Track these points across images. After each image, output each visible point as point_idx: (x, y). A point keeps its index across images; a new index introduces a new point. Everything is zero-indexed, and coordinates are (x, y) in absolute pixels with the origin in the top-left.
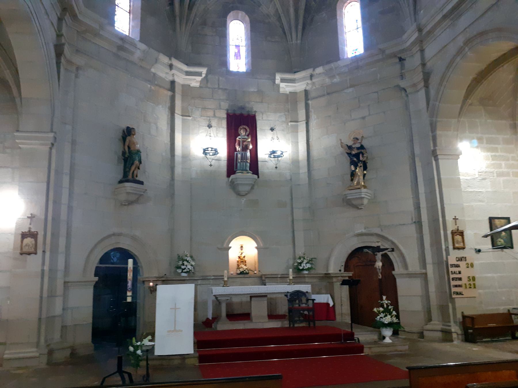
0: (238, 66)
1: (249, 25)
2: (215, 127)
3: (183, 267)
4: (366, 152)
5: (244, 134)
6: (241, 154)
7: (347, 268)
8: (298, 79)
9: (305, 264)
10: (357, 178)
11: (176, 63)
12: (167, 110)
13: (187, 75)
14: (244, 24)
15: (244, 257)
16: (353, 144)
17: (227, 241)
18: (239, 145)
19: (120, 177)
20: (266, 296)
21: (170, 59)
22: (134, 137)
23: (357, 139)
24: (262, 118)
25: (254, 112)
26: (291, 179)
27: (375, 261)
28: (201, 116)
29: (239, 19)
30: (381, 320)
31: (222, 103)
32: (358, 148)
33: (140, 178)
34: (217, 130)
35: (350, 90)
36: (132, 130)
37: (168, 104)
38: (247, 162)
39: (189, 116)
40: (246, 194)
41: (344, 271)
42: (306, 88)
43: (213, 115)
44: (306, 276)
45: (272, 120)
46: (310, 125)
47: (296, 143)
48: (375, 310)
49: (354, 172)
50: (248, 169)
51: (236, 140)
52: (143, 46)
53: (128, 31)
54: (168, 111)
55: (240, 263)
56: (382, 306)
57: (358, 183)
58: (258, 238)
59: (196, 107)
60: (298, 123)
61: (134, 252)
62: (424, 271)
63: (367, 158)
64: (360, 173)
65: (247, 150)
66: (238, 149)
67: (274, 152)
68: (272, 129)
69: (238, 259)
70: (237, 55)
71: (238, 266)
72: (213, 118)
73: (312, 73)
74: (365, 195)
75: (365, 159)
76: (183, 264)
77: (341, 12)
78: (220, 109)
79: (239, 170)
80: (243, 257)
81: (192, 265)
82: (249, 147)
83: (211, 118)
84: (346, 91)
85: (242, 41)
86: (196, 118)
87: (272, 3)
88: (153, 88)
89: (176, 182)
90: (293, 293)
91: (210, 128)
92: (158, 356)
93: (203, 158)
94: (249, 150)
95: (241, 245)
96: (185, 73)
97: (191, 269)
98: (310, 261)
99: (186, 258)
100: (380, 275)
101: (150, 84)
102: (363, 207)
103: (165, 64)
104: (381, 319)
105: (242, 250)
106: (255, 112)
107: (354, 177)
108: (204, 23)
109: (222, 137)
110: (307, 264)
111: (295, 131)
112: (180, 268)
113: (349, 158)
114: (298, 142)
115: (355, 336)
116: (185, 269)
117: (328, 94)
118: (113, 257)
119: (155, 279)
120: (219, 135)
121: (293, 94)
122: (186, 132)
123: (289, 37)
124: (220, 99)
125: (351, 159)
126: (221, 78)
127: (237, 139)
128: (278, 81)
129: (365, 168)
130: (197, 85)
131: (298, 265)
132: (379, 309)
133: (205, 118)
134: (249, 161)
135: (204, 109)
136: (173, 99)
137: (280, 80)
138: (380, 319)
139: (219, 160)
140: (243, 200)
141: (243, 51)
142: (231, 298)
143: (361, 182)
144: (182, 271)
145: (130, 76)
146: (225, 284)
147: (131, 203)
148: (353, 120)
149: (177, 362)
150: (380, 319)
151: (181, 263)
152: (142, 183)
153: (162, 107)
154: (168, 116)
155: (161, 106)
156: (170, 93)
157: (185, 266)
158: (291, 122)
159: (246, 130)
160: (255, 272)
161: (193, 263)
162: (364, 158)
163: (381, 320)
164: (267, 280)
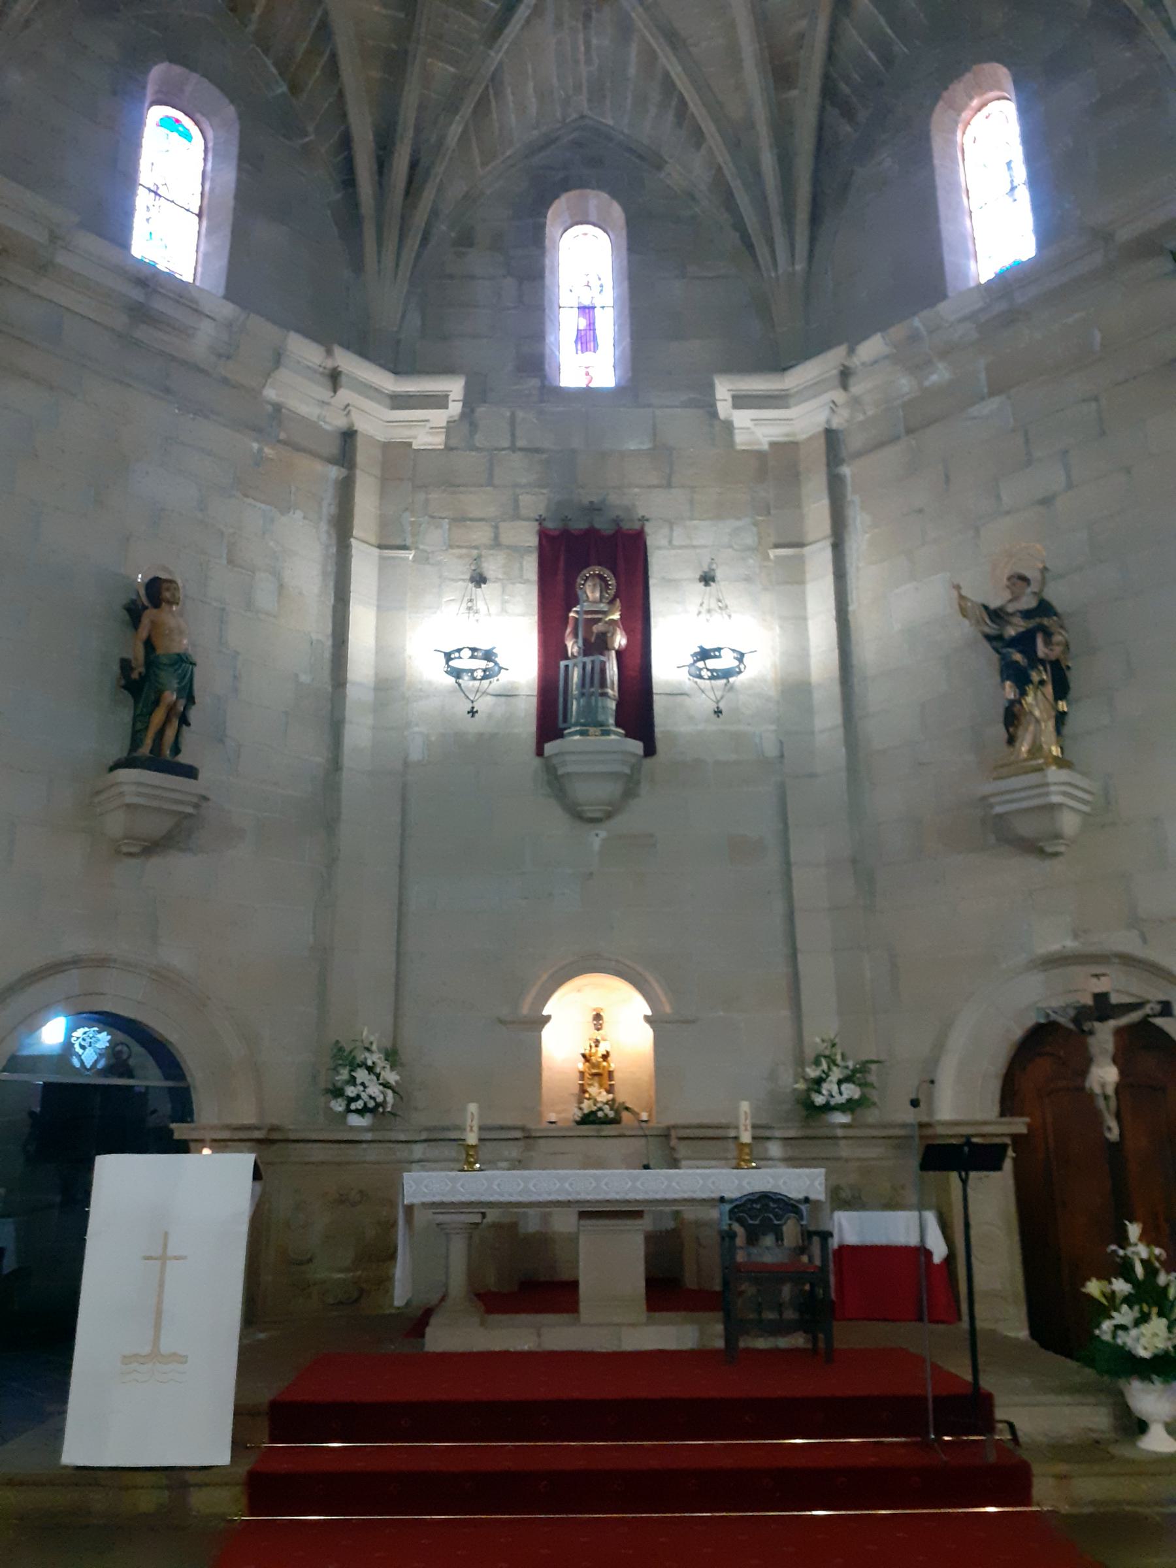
0: (587, 374)
1: (624, 233)
2: (497, 580)
4: (1062, 627)
5: (597, 595)
6: (581, 665)
7: (1010, 1102)
8: (797, 392)
9: (835, 1088)
10: (1031, 728)
11: (348, 362)
12: (324, 527)
13: (393, 408)
14: (610, 233)
15: (605, 1057)
16: (1010, 601)
17: (533, 992)
19: (118, 749)
20: (638, 1214)
21: (329, 353)
22: (171, 612)
23: (1024, 579)
24: (670, 542)
25: (639, 520)
26: (782, 756)
27: (1087, 1062)
28: (451, 547)
29: (593, 218)
30: (1123, 1339)
31: (526, 500)
32: (1027, 614)
33: (183, 758)
34: (504, 591)
35: (993, 404)
36: (165, 585)
37: (328, 507)
38: (605, 695)
39: (404, 547)
40: (609, 816)
41: (1003, 1114)
42: (828, 421)
44: (840, 1132)
45: (705, 547)
46: (847, 551)
47: (797, 621)
48: (1094, 1287)
49: (1017, 707)
50: (611, 721)
51: (567, 617)
53: (193, 272)
54: (328, 532)
55: (590, 1082)
56: (1125, 1270)
57: (1036, 750)
58: (651, 979)
59: (432, 517)
60: (807, 550)
61: (161, 1031)
63: (1067, 646)
64: (1041, 712)
65: (610, 652)
66: (572, 648)
67: (704, 654)
68: (707, 579)
69: (581, 1065)
70: (586, 340)
71: (583, 1090)
72: (491, 552)
73: (846, 363)
74: (1065, 794)
75: (1056, 652)
76: (352, 1081)
77: (951, 142)
78: (516, 516)
79: (576, 725)
80: (600, 1054)
81: (386, 1085)
82: (613, 642)
83: (484, 552)
84: (974, 411)
85: (601, 290)
86: (433, 552)
87: (703, 151)
88: (268, 451)
89: (345, 774)
90: (743, 1205)
91: (480, 587)
92: (78, 1468)
93: (453, 691)
94: (613, 653)
95: (594, 1010)
96: (388, 401)
97: (380, 1099)
98: (854, 1071)
99: (361, 1056)
100: (1113, 1123)
101: (256, 440)
102: (1062, 849)
103: (315, 371)
104: (1120, 1333)
105: (598, 1029)
106: (644, 519)
107: (1016, 727)
108: (466, 240)
109: (523, 615)
110: (844, 1087)
112: (338, 1092)
113: (997, 656)
114: (804, 619)
115: (999, 1414)
116: (358, 1097)
117: (910, 431)
118: (83, 1047)
119: (226, 1135)
120: (510, 607)
123: (762, 251)
124: (516, 486)
125: (1004, 658)
126: (520, 414)
127: (572, 614)
128: (724, 408)
129: (1061, 689)
130: (437, 441)
131: (809, 1090)
132: (1110, 1283)
133: (464, 551)
134: (613, 692)
135: (460, 520)
136: (345, 491)
137: (730, 399)
138: (1114, 1336)
139: (507, 695)
140: (597, 838)
141: (607, 325)
142: (545, 1218)
143: (1045, 746)
144: (348, 1105)
145: (179, 409)
146: (468, 1158)
147: (152, 847)
148: (1008, 513)
149: (147, 1501)
150: (1114, 1336)
151: (344, 1074)
152: (190, 772)
153: (304, 518)
154: (327, 547)
155: (299, 514)
156: (334, 472)
157: (361, 1088)
159: (601, 577)
160: (644, 1116)
161: (392, 1077)
162: (1051, 650)
163: (1119, 1341)
164: (683, 1149)
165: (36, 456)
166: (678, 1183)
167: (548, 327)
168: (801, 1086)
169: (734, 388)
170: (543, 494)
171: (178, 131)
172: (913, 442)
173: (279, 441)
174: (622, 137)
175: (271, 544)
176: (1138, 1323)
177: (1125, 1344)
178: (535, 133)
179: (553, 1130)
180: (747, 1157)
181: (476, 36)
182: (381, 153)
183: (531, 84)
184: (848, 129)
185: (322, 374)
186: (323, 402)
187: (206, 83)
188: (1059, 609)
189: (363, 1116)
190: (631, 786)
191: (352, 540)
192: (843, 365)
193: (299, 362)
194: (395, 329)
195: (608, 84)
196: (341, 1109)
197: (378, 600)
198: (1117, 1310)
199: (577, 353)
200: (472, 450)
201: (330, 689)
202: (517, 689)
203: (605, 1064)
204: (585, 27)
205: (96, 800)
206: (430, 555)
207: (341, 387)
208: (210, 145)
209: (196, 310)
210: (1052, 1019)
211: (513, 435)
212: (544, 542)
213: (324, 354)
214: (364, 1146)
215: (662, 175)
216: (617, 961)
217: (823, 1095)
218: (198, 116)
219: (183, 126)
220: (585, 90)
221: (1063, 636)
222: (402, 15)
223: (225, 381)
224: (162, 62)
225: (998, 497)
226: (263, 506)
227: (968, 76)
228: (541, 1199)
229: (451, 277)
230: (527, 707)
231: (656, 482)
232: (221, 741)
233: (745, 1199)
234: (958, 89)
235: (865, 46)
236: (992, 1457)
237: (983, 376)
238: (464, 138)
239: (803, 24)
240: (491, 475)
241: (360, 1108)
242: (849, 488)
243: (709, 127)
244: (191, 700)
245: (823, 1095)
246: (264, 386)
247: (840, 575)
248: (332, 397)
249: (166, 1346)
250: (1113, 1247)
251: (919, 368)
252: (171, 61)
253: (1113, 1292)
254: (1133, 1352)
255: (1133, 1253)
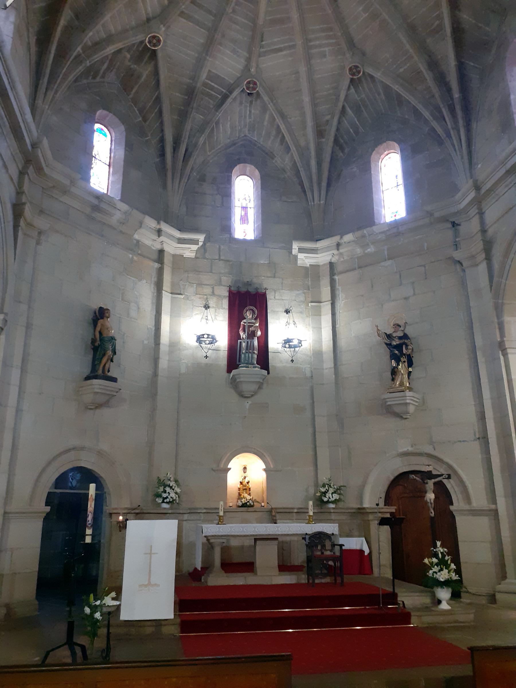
0: (245, 232)
3: (164, 495)
4: (411, 343)
7: (388, 501)
9: (331, 495)
10: (400, 376)
11: (165, 227)
12: (153, 286)
15: (248, 483)
18: (244, 331)
19: (87, 371)
20: (276, 539)
21: (159, 223)
24: (275, 298)
26: (312, 376)
28: (196, 294)
29: (248, 174)
32: (400, 338)
34: (215, 312)
35: (389, 263)
37: (154, 279)
38: (254, 353)
40: (252, 396)
41: (385, 505)
43: (211, 293)
44: (332, 511)
47: (318, 329)
49: (396, 369)
50: (255, 363)
52: (124, 207)
54: (154, 288)
56: (436, 555)
57: (402, 384)
58: (267, 457)
59: (190, 283)
60: (321, 304)
62: (493, 507)
64: (403, 371)
68: (287, 312)
69: (239, 486)
70: (244, 219)
71: (240, 495)
73: (339, 242)
74: (411, 400)
76: (165, 492)
77: (377, 166)
79: (243, 364)
80: (246, 482)
81: (176, 493)
82: (257, 334)
83: (209, 297)
84: (383, 264)
86: (190, 296)
88: (135, 258)
89: (159, 378)
93: (197, 347)
96: (177, 241)
98: (337, 489)
101: (131, 254)
102: (408, 417)
103: (152, 229)
105: (245, 473)
106: (266, 289)
107: (395, 375)
108: (202, 179)
109: (222, 321)
111: (317, 313)
112: (159, 496)
114: (321, 328)
116: (167, 498)
117: (360, 267)
120: (218, 318)
121: (315, 267)
122: (175, 314)
124: (220, 273)
128: (295, 251)
129: (410, 364)
135: (200, 284)
136: (160, 272)
137: (297, 249)
139: (217, 350)
140: (248, 403)
141: (251, 214)
142: (228, 540)
145: (106, 243)
146: (221, 521)
147: (99, 406)
148: (393, 301)
149: (149, 630)
151: (161, 489)
152: (114, 380)
154: (154, 293)
155: (144, 281)
156: (157, 265)
158: (312, 302)
159: (252, 310)
161: (178, 490)
164: (278, 516)
165: (61, 262)
166: (292, 529)
167: (232, 215)
168: (318, 494)
169: (299, 245)
170: (230, 277)
171: (102, 133)
172: (361, 271)
173: (139, 254)
174: (260, 145)
175: (136, 292)
176: (439, 571)
177: (436, 577)
178: (229, 140)
179: (232, 509)
180: (312, 520)
181: (212, 106)
182: (174, 145)
183: (229, 123)
184: (341, 154)
185: (155, 230)
186: (154, 240)
187: (114, 117)
188: (410, 338)
189: (169, 504)
190: (260, 386)
191: (163, 291)
192: (338, 242)
193: (147, 226)
194: (178, 212)
195: (256, 126)
196: (161, 502)
197: (171, 313)
198: (434, 567)
199: (241, 224)
200: (205, 259)
201: (154, 346)
202: (220, 348)
203: (248, 485)
204: (250, 106)
205: (81, 389)
206: (189, 297)
207: (162, 236)
208: (113, 139)
209: (115, 208)
210: (414, 478)
211: (220, 255)
212: (231, 295)
213: (157, 223)
214: (168, 515)
215: (274, 161)
216: (255, 449)
217: (326, 497)
218: (109, 128)
219: (104, 131)
220: (247, 126)
221: (411, 346)
222: (187, 97)
223: (121, 232)
224: (100, 109)
225: (390, 295)
226: (133, 278)
227: (385, 144)
228: (248, 534)
229: (197, 193)
230: (224, 354)
231: (269, 275)
232: (119, 366)
233: (313, 534)
234: (381, 148)
235: (349, 127)
236: (400, 611)
237: (386, 253)
238: (205, 143)
239: (328, 117)
240: (211, 269)
241: (168, 501)
242: (337, 284)
243: (293, 148)
244: (115, 353)
245: (326, 497)
246: (135, 234)
247: (333, 314)
248: (157, 238)
249: (153, 581)
250: (432, 549)
251: (365, 246)
252: (104, 109)
253: (433, 562)
254: (439, 579)
255: (438, 550)
